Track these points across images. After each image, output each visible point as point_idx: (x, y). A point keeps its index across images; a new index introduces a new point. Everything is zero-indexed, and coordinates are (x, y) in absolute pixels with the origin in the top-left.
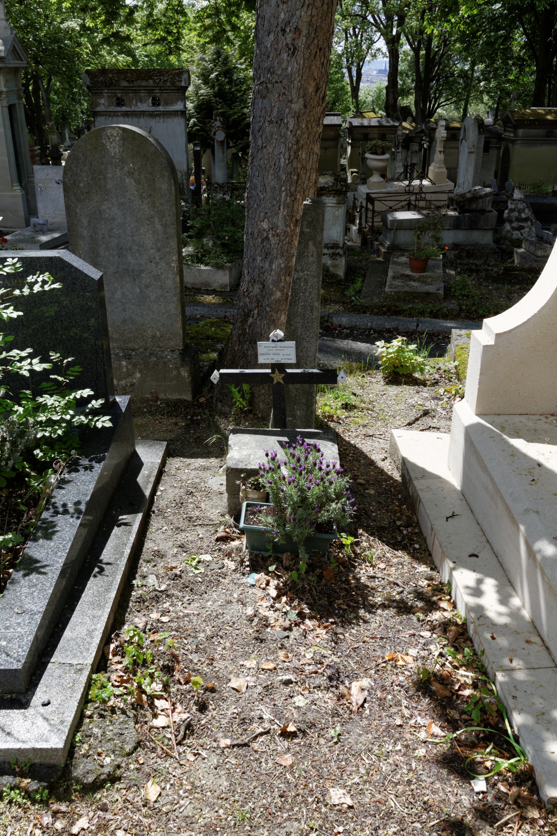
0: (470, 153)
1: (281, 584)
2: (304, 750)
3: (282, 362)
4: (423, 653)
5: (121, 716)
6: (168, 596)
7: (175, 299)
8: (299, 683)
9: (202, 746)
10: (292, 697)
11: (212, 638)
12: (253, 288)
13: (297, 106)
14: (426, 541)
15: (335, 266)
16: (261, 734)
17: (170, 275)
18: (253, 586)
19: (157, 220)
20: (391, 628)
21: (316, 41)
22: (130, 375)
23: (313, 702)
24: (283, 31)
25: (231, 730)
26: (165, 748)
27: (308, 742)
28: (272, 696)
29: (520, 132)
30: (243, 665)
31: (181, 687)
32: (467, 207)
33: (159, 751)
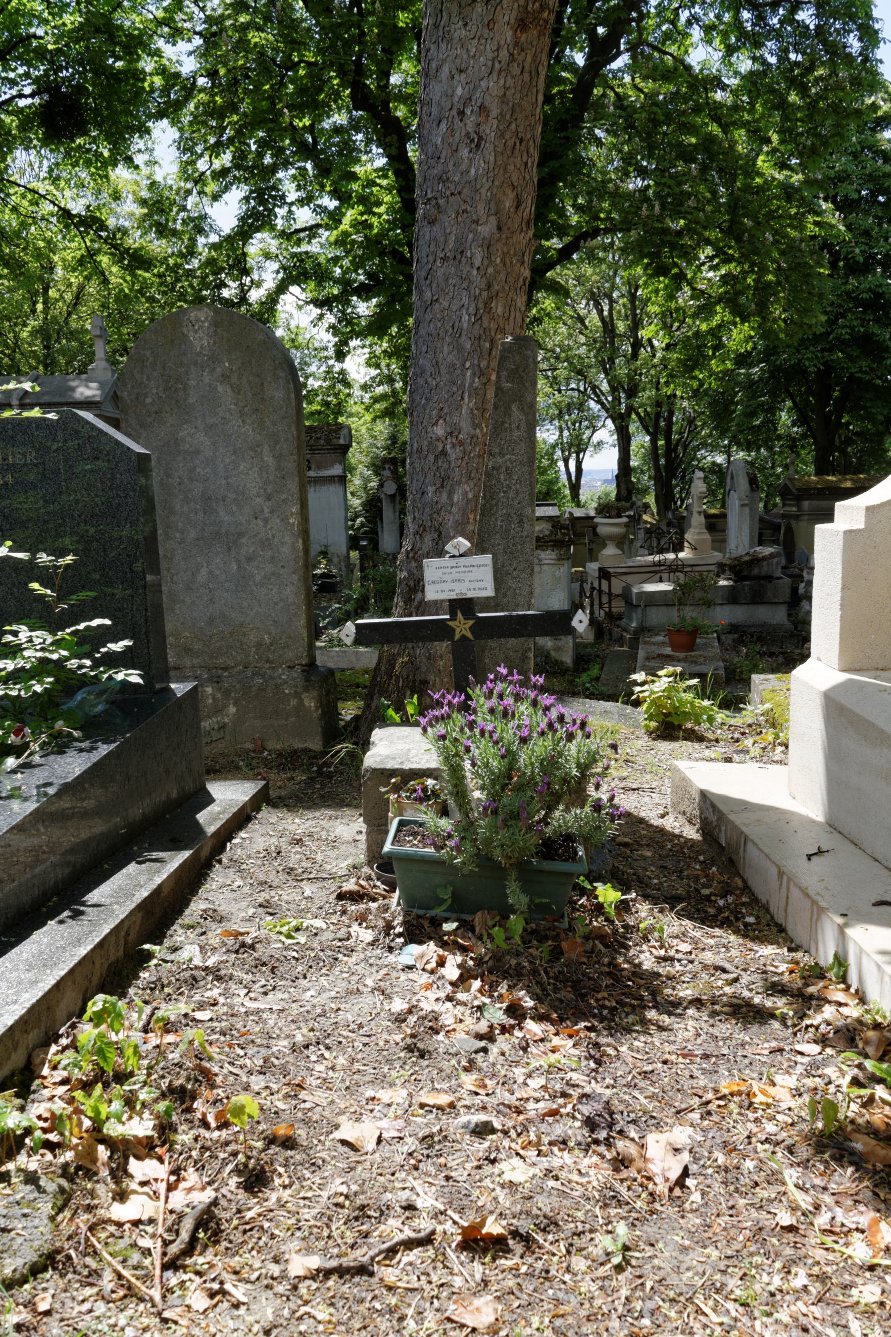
0: (743, 505)
1: (471, 963)
2: (529, 1287)
3: (469, 595)
4: (810, 1082)
5: (22, 1187)
6: (219, 978)
7: (295, 577)
8: (513, 1133)
9: (236, 1273)
10: (493, 1162)
11: (307, 1047)
12: (423, 542)
13: (487, 229)
14: (767, 910)
15: (558, 649)
16: (409, 1244)
17: (287, 539)
18: (410, 968)
19: (266, 448)
20: (724, 1039)
21: (513, 126)
22: (218, 710)
23: (548, 1172)
24: (461, 113)
25: (325, 1233)
26: (126, 1273)
27: (539, 1265)
28: (442, 1160)
29: (806, 504)
30: (373, 1099)
31: (207, 1134)
32: (745, 573)
33: (107, 1282)
